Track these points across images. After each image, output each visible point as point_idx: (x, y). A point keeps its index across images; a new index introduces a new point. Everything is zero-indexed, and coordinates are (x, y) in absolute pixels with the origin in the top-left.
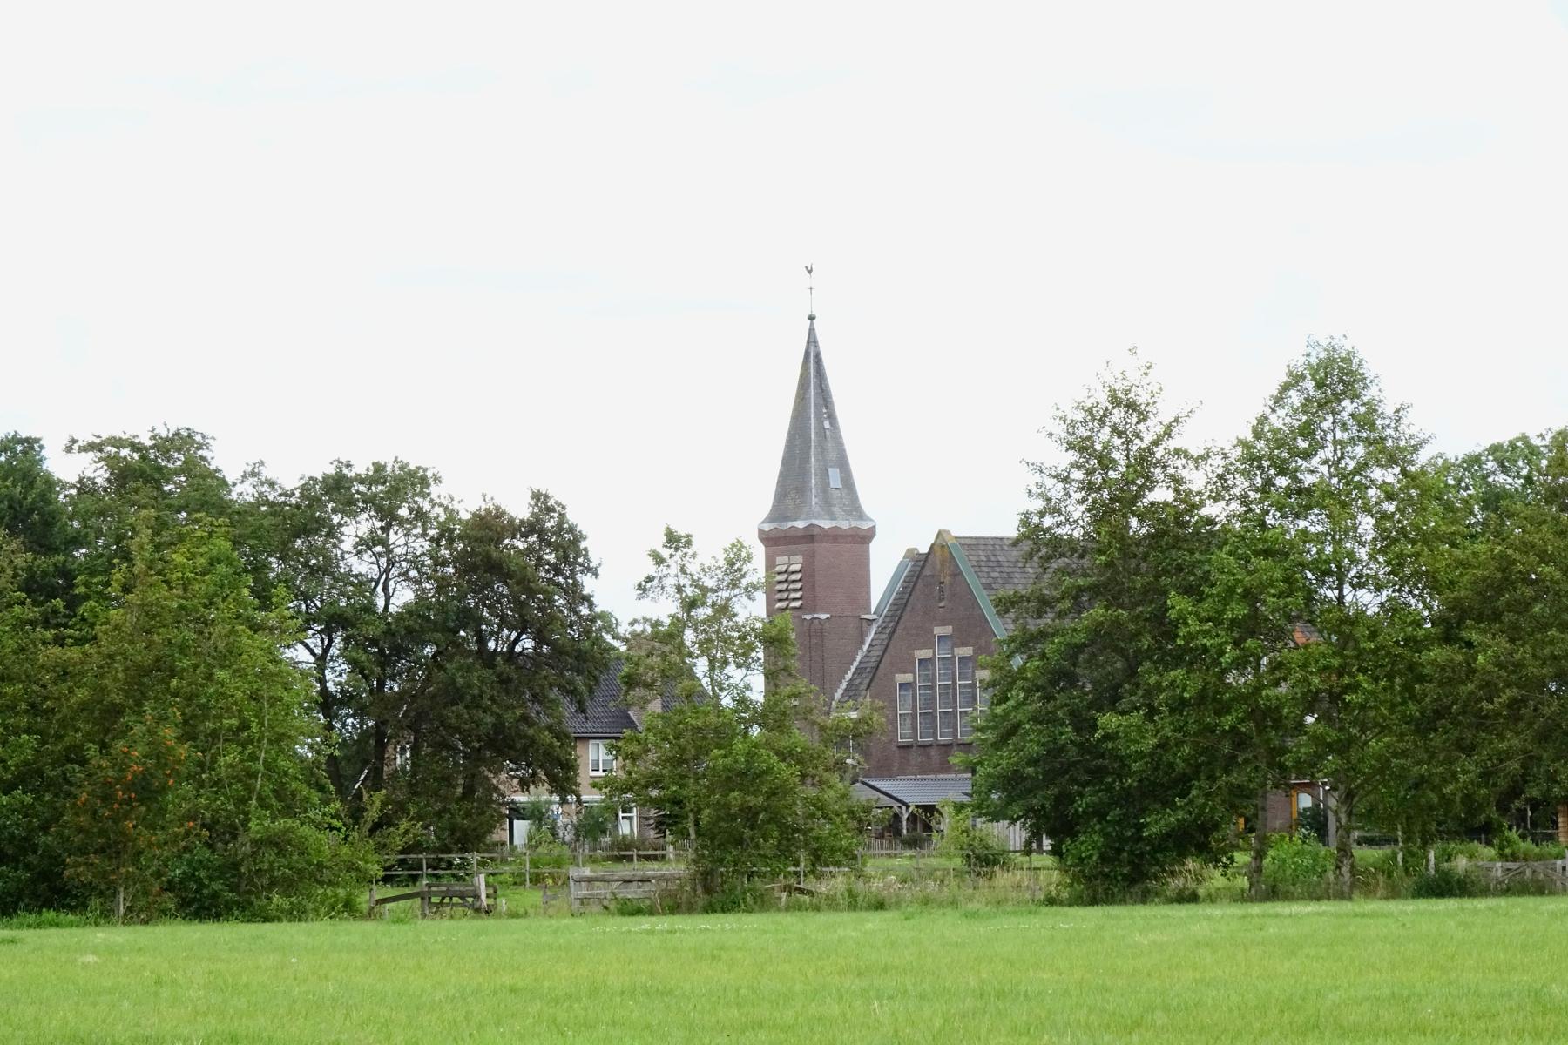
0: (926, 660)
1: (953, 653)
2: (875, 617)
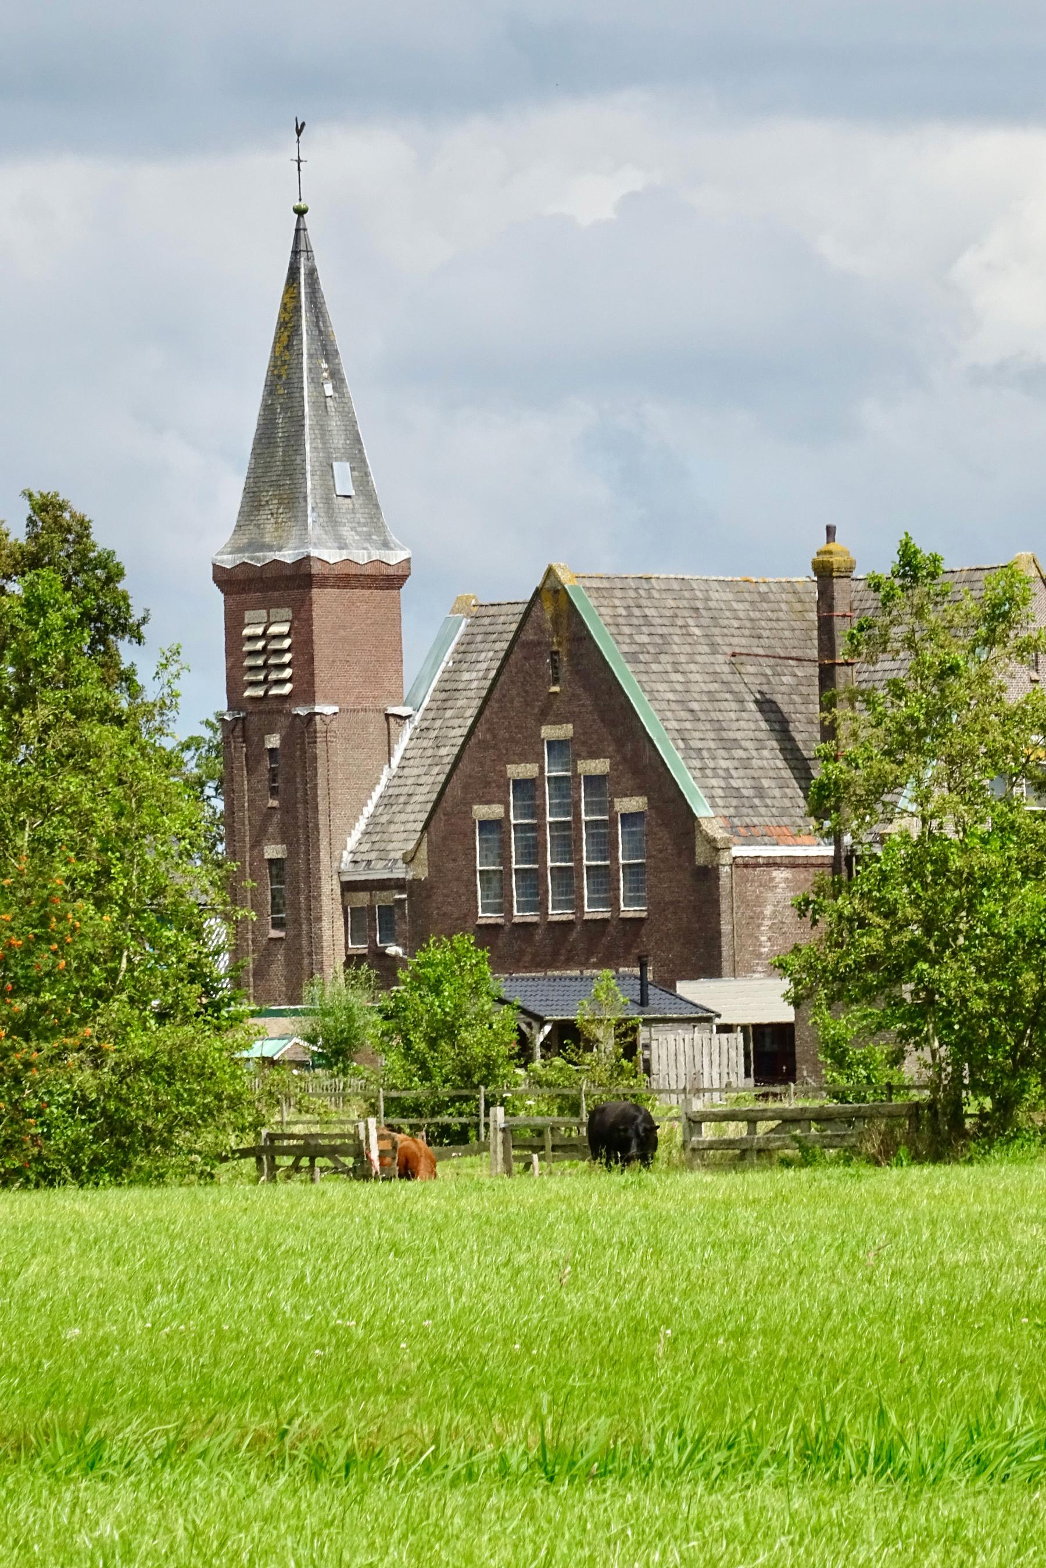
0: (525, 781)
1: (575, 770)
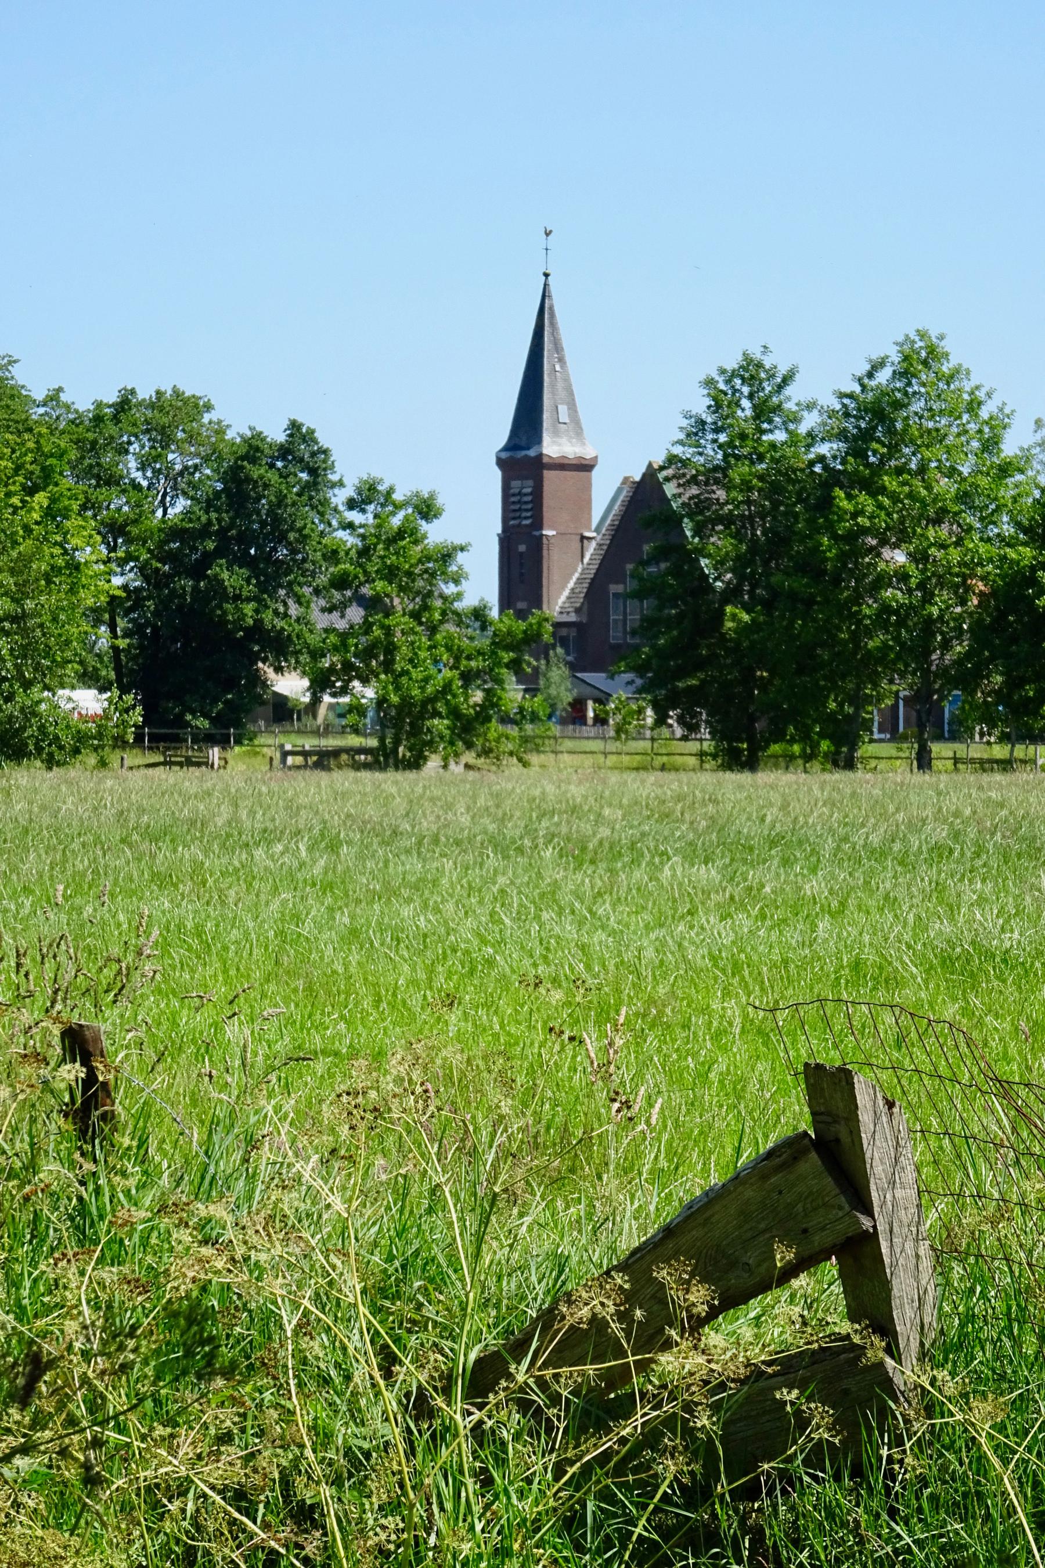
2: (594, 534)
